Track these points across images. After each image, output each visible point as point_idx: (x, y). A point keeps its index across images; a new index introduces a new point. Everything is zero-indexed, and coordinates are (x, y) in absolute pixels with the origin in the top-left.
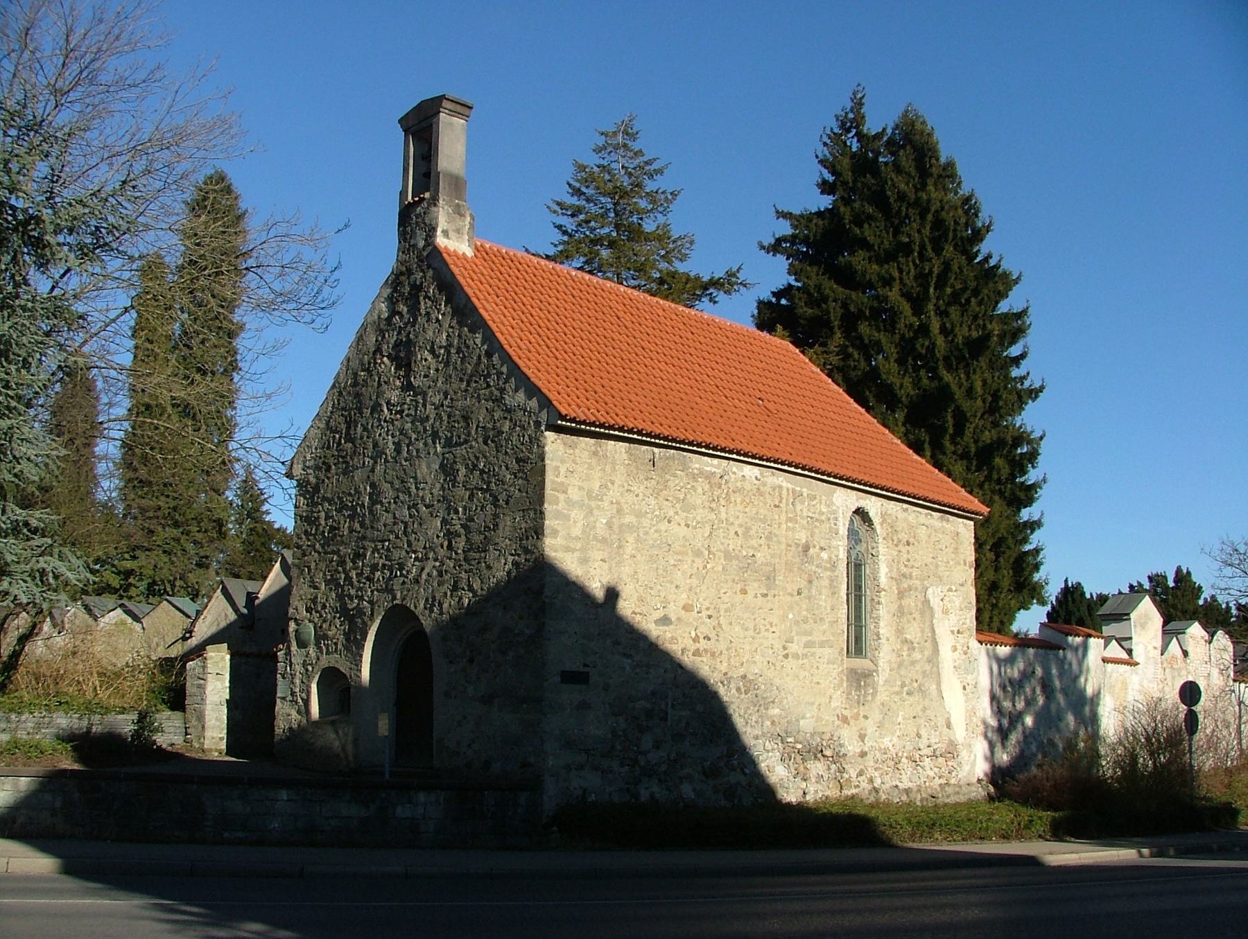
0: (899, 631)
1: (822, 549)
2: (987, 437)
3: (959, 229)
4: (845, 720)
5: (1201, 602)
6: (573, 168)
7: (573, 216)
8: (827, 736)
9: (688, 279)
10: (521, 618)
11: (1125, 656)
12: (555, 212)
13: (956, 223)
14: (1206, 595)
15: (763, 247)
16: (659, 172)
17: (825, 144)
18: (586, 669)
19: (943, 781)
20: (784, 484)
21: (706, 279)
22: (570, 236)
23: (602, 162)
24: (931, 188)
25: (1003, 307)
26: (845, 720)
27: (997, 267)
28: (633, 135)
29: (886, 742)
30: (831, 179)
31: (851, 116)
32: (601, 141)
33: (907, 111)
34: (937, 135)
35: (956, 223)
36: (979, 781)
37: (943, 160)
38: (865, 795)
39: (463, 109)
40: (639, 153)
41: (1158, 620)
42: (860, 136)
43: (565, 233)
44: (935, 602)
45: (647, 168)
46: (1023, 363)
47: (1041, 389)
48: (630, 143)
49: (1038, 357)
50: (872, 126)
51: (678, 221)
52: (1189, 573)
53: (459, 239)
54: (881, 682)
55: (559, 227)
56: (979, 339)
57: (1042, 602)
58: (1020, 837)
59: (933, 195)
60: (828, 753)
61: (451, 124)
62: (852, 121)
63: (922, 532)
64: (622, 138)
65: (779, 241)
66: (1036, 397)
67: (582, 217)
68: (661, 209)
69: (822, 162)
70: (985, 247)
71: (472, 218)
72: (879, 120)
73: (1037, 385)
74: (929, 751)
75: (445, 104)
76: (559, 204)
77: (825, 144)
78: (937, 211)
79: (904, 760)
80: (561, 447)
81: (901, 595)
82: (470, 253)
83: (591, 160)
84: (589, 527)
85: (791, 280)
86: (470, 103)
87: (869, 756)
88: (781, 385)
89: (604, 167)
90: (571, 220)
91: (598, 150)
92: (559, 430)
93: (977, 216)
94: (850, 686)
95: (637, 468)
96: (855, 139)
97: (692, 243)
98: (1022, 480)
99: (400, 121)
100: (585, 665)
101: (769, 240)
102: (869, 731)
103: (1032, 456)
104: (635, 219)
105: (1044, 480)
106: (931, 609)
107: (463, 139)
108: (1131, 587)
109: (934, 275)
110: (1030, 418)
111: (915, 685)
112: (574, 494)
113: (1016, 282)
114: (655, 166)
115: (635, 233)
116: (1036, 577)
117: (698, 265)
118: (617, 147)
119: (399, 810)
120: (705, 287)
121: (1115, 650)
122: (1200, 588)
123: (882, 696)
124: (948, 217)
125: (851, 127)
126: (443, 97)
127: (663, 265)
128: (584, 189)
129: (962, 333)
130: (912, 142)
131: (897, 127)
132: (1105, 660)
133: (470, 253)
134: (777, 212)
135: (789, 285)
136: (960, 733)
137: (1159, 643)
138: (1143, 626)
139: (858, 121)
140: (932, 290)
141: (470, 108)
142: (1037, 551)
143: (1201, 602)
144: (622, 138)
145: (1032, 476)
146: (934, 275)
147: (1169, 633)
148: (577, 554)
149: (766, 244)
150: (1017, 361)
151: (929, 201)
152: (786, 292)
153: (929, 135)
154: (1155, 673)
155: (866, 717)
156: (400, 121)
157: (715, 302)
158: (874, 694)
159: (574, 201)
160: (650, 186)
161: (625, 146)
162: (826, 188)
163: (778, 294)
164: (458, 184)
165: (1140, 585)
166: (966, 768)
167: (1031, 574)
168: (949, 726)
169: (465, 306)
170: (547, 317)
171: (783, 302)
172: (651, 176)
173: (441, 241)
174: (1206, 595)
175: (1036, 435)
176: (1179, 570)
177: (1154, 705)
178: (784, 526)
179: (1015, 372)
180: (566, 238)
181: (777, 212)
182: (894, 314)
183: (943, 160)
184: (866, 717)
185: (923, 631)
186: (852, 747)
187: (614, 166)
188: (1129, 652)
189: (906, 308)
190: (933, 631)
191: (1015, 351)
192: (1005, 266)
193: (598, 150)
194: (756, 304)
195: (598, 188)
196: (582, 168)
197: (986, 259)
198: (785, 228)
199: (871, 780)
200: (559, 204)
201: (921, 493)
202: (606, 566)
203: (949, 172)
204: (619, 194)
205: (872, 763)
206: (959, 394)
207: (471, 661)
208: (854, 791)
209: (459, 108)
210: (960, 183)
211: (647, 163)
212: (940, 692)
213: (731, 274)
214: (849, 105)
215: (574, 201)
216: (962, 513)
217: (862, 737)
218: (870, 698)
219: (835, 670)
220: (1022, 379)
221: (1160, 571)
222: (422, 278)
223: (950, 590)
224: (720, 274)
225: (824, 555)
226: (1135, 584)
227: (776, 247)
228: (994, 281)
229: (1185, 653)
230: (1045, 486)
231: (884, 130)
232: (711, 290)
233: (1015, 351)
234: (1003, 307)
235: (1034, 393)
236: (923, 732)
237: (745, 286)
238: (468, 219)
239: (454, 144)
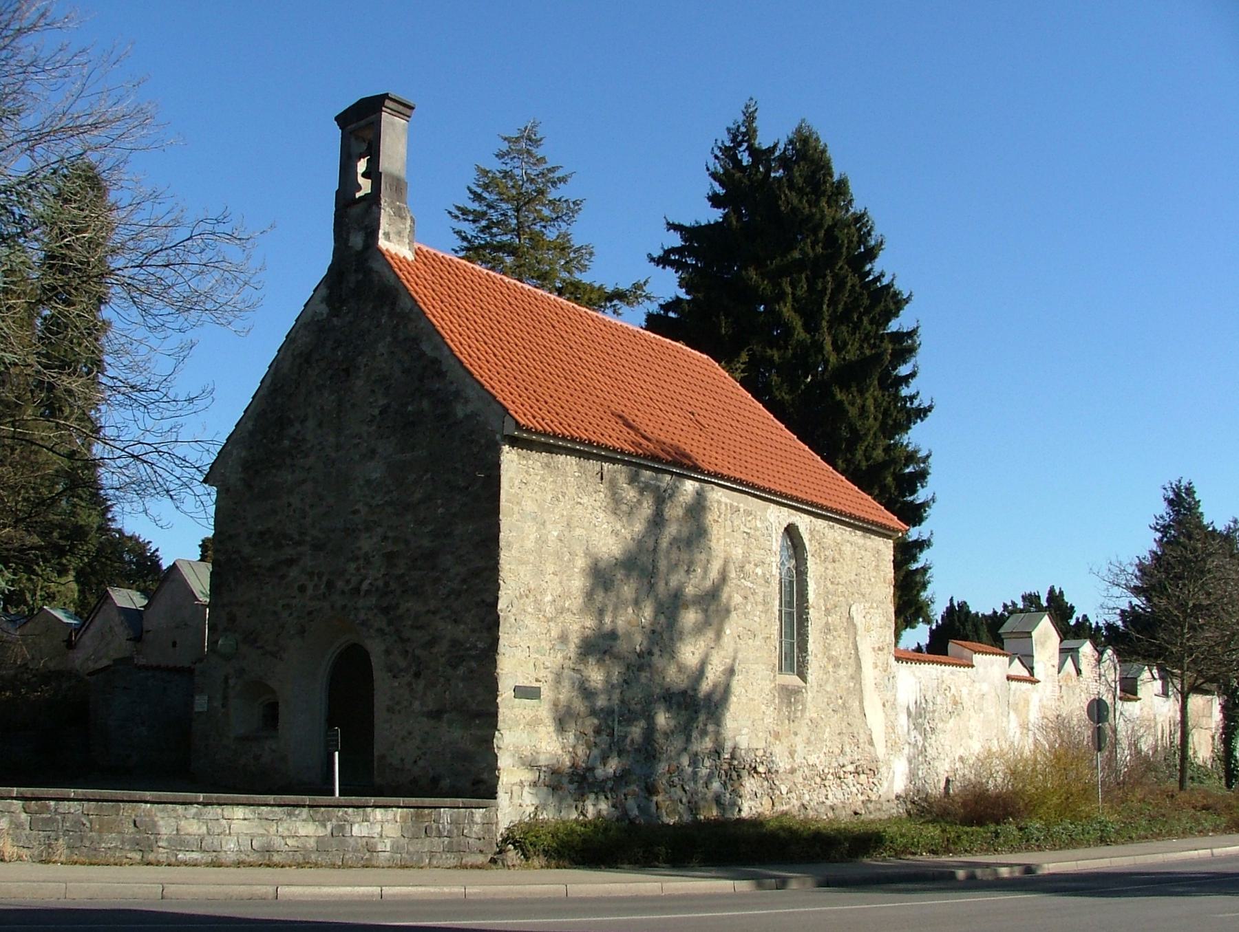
0: (827, 648)
1: (756, 565)
2: (879, 454)
3: (851, 246)
4: (777, 736)
5: (1072, 622)
6: (475, 173)
7: (474, 221)
8: (760, 753)
9: (592, 289)
10: (473, 631)
11: (1025, 673)
12: (456, 217)
13: (851, 242)
14: (1078, 614)
15: (652, 259)
16: (563, 180)
17: (716, 157)
18: (537, 685)
19: (864, 798)
20: (724, 499)
21: (609, 289)
22: (469, 242)
23: (504, 167)
24: (823, 203)
25: (894, 326)
26: (777, 736)
27: (888, 287)
28: (537, 141)
29: (812, 759)
30: (721, 191)
31: (743, 129)
32: (505, 147)
33: (801, 127)
34: (831, 153)
35: (851, 242)
36: (898, 797)
37: (836, 178)
38: (795, 812)
39: (405, 109)
40: (542, 160)
41: (1054, 638)
42: (752, 151)
43: (465, 239)
44: (858, 619)
45: (551, 175)
46: (913, 382)
47: (930, 409)
48: (534, 150)
49: (926, 378)
50: (763, 141)
51: (579, 233)
52: (1061, 593)
53: (400, 242)
54: (809, 699)
55: (458, 233)
56: (872, 356)
57: (928, 621)
58: (947, 851)
59: (826, 211)
60: (761, 769)
61: (393, 124)
62: (744, 135)
63: (847, 549)
64: (525, 143)
65: (668, 252)
66: (925, 416)
67: (484, 223)
68: (566, 218)
69: (714, 175)
70: (877, 266)
71: (413, 220)
72: (773, 133)
73: (926, 404)
74: (851, 768)
75: (387, 103)
76: (458, 208)
77: (716, 157)
78: (829, 227)
79: (830, 776)
80: (516, 457)
81: (828, 612)
82: (410, 256)
83: (495, 166)
84: (541, 541)
85: (682, 294)
86: (411, 102)
87: (799, 773)
88: (707, 399)
89: (506, 172)
90: (472, 226)
91: (500, 156)
92: (515, 442)
93: (870, 235)
94: (781, 702)
95: (586, 480)
96: (747, 153)
97: (591, 254)
98: (910, 498)
99: (336, 119)
100: (537, 680)
101: (658, 253)
102: (799, 748)
103: (922, 475)
104: (537, 228)
105: (933, 500)
106: (854, 626)
107: (404, 140)
108: (1005, 606)
109: (829, 291)
110: (916, 437)
111: (840, 701)
112: (529, 506)
113: (907, 301)
114: (558, 174)
115: (536, 241)
116: (924, 595)
117: (597, 275)
118: (520, 152)
119: (356, 828)
120: (610, 298)
121: (1018, 669)
122: (1072, 608)
123: (811, 713)
124: (842, 235)
125: (743, 141)
126: (386, 96)
127: (564, 275)
128: (485, 195)
129: (852, 354)
130: (806, 156)
131: (791, 142)
132: (1009, 678)
133: (410, 256)
134: (668, 224)
135: (678, 297)
136: (881, 750)
137: (1056, 661)
138: (1043, 644)
139: (750, 133)
140: (825, 307)
141: (412, 108)
142: (924, 570)
143: (1072, 622)
144: (525, 143)
145: (921, 496)
146: (829, 291)
147: (1067, 652)
148: (530, 567)
149: (655, 256)
150: (906, 379)
151: (823, 217)
152: (676, 304)
153: (824, 151)
154: (1053, 691)
155: (796, 734)
156: (336, 119)
157: (619, 314)
158: (803, 711)
159: (475, 206)
160: (553, 194)
161: (528, 152)
162: (715, 201)
163: (666, 307)
164: (399, 186)
165: (1014, 604)
166: (885, 784)
167: (919, 592)
168: (871, 743)
169: (411, 310)
170: (483, 326)
171: (672, 315)
172: (554, 183)
173: (383, 243)
174: (1078, 614)
175: (922, 454)
176: (1052, 591)
177: (1060, 725)
178: (722, 542)
179: (905, 392)
180: (465, 244)
181: (668, 224)
182: (788, 330)
183: (836, 178)
184: (796, 734)
185: (846, 648)
186: (783, 764)
187: (516, 172)
188: (1031, 670)
189: (798, 323)
190: (856, 649)
191: (904, 370)
192: (898, 286)
193: (500, 156)
194: (645, 317)
195: (500, 194)
196: (485, 173)
197: (878, 279)
198: (676, 240)
199: (799, 798)
200: (458, 208)
201: (848, 510)
202: (557, 579)
203: (841, 188)
204: (522, 202)
205: (801, 780)
206: (853, 412)
207: (417, 675)
208: (785, 808)
209: (401, 108)
210: (851, 201)
211: (549, 170)
212: (862, 709)
213: (638, 286)
214: (741, 118)
215: (475, 206)
216: (881, 531)
217: (792, 754)
218: (799, 714)
219: (767, 686)
220: (912, 398)
221: (1033, 591)
222: (358, 278)
223: (871, 607)
224: (624, 286)
225: (759, 571)
226: (1009, 603)
227: (663, 260)
228: (888, 301)
229: (1079, 672)
230: (934, 506)
231: (775, 146)
232: (615, 302)
233: (904, 370)
234: (894, 326)
235: (922, 413)
236: (847, 749)
237: (649, 298)
238: (409, 222)
239: (395, 140)
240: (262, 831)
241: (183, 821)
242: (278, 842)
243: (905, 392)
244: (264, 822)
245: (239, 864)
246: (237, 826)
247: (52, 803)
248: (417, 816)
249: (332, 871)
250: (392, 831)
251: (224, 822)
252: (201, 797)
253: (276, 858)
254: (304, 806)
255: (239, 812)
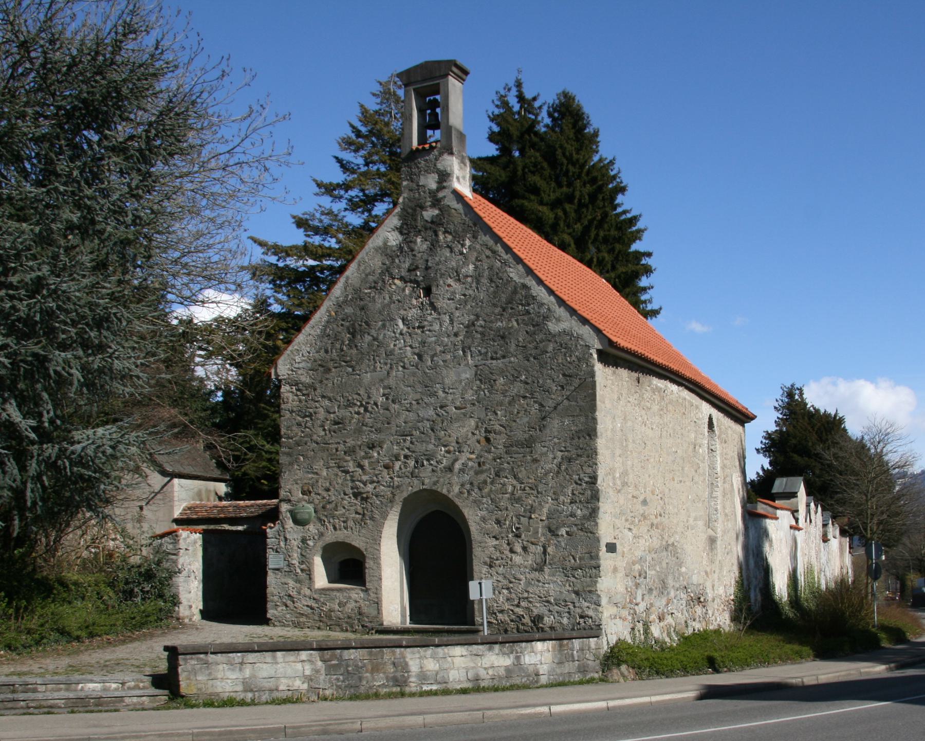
0: (724, 507)
18: (614, 541)
20: (687, 397)
107: (461, 100)
130: (568, 112)
150: (644, 289)
162: (492, 138)
197: (625, 212)
240: (472, 665)
241: (748, 672)
242: (482, 673)
243: (644, 297)
244: (474, 657)
245: (464, 691)
246: (458, 661)
247: (339, 651)
248: (561, 646)
249: (497, 694)
250: (548, 658)
251: (449, 659)
252: (437, 641)
253: (482, 684)
254: (496, 643)
255: (458, 650)
